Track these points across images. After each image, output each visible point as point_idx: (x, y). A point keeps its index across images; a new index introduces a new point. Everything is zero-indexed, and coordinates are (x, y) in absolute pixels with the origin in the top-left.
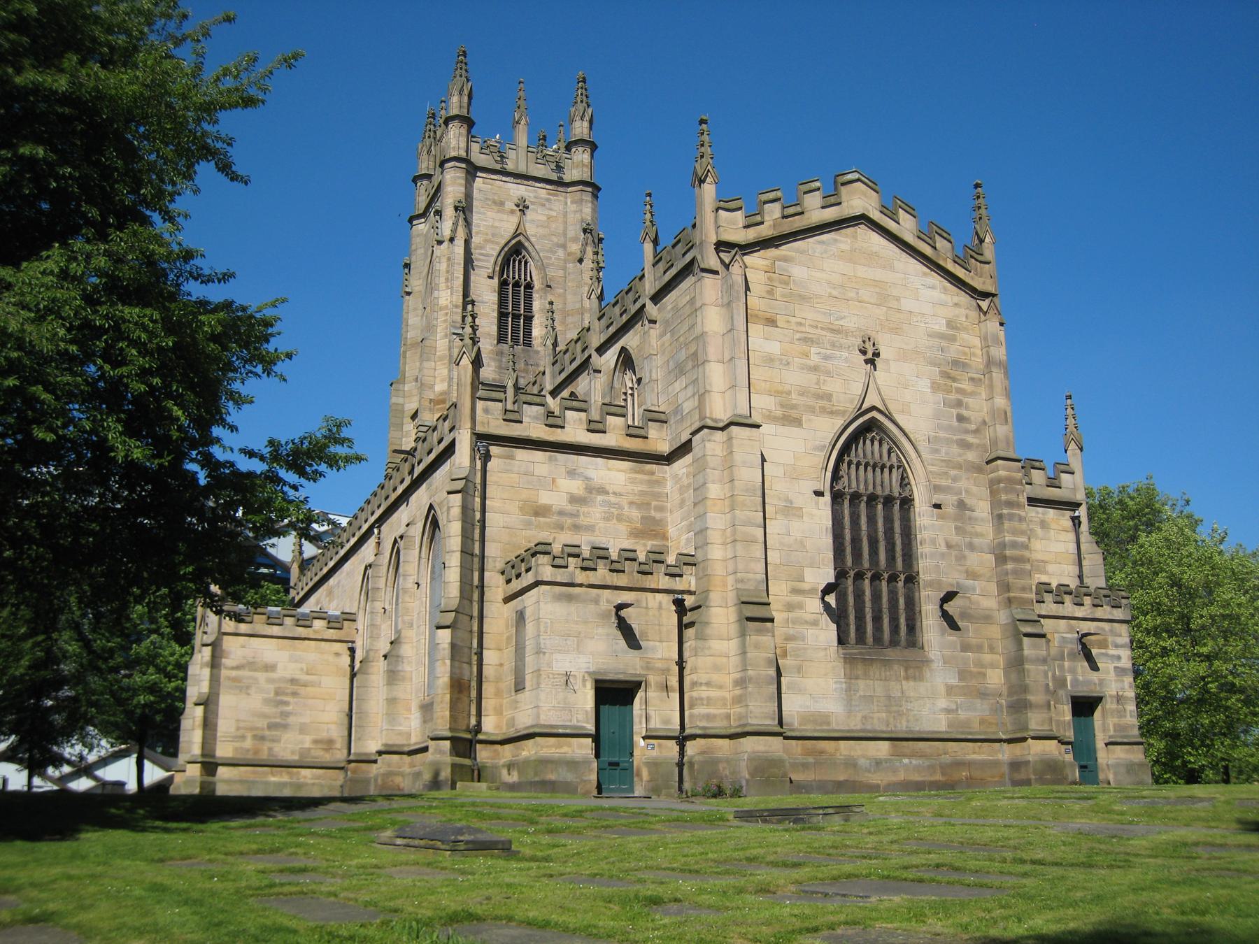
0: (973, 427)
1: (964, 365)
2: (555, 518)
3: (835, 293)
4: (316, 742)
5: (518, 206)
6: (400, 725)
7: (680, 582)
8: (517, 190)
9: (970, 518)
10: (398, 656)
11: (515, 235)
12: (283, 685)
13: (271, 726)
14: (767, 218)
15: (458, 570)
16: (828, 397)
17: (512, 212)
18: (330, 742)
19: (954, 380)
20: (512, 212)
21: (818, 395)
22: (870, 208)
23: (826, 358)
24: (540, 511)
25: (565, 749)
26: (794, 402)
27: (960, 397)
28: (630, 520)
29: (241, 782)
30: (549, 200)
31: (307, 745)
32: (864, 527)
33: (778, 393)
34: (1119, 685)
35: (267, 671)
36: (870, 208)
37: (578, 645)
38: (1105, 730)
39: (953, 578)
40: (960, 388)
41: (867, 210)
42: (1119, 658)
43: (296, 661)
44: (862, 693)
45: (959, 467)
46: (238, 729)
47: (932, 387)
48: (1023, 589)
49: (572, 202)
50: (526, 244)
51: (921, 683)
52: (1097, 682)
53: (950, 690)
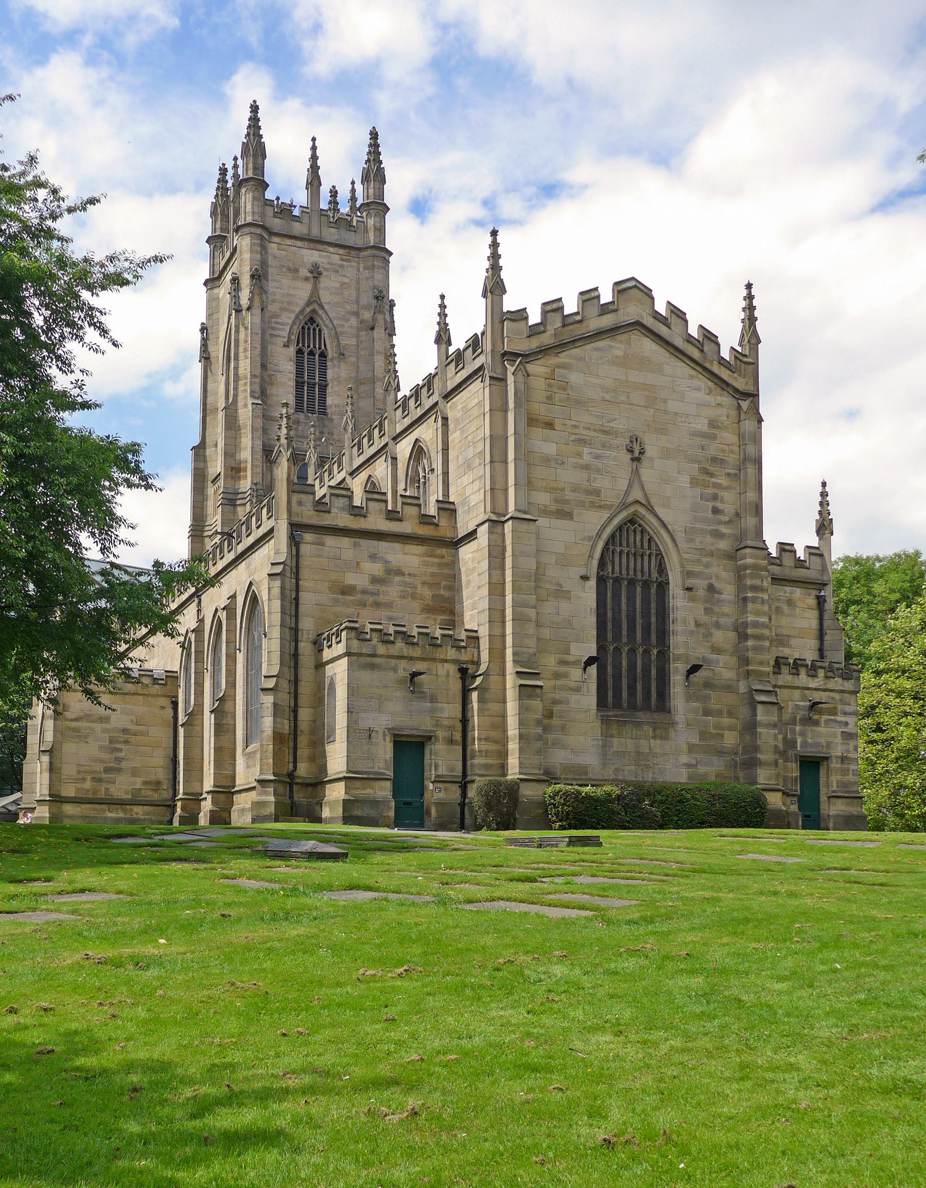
0: (727, 519)
1: (722, 461)
2: (359, 596)
3: (607, 397)
4: (145, 783)
5: (311, 272)
6: (226, 770)
7: (466, 653)
8: (311, 256)
9: (718, 601)
10: (223, 712)
11: (309, 303)
12: (115, 735)
13: (107, 770)
14: (549, 328)
15: (278, 641)
16: (597, 492)
17: (307, 279)
18: (158, 783)
19: (712, 475)
20: (307, 279)
21: (588, 491)
22: (644, 314)
23: (597, 457)
24: (347, 590)
25: (369, 791)
26: (567, 497)
27: (716, 491)
28: (422, 598)
29: (84, 817)
30: (342, 266)
31: (138, 786)
32: (624, 607)
33: (553, 490)
34: (845, 747)
35: (102, 722)
36: (644, 314)
37: (379, 706)
38: (828, 785)
39: (699, 652)
40: (717, 483)
41: (642, 317)
42: (846, 724)
43: (127, 714)
44: (615, 749)
45: (711, 554)
46: (79, 772)
47: (691, 483)
48: (761, 663)
49: (365, 269)
50: (320, 312)
51: (667, 742)
52: (824, 744)
53: (691, 748)
